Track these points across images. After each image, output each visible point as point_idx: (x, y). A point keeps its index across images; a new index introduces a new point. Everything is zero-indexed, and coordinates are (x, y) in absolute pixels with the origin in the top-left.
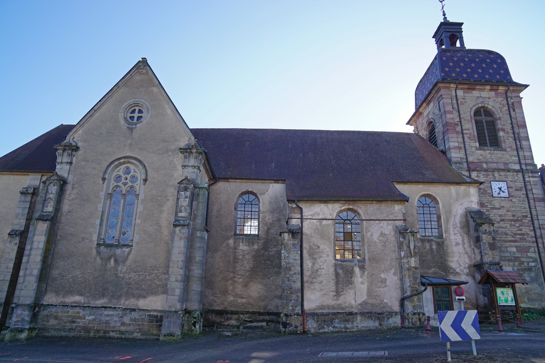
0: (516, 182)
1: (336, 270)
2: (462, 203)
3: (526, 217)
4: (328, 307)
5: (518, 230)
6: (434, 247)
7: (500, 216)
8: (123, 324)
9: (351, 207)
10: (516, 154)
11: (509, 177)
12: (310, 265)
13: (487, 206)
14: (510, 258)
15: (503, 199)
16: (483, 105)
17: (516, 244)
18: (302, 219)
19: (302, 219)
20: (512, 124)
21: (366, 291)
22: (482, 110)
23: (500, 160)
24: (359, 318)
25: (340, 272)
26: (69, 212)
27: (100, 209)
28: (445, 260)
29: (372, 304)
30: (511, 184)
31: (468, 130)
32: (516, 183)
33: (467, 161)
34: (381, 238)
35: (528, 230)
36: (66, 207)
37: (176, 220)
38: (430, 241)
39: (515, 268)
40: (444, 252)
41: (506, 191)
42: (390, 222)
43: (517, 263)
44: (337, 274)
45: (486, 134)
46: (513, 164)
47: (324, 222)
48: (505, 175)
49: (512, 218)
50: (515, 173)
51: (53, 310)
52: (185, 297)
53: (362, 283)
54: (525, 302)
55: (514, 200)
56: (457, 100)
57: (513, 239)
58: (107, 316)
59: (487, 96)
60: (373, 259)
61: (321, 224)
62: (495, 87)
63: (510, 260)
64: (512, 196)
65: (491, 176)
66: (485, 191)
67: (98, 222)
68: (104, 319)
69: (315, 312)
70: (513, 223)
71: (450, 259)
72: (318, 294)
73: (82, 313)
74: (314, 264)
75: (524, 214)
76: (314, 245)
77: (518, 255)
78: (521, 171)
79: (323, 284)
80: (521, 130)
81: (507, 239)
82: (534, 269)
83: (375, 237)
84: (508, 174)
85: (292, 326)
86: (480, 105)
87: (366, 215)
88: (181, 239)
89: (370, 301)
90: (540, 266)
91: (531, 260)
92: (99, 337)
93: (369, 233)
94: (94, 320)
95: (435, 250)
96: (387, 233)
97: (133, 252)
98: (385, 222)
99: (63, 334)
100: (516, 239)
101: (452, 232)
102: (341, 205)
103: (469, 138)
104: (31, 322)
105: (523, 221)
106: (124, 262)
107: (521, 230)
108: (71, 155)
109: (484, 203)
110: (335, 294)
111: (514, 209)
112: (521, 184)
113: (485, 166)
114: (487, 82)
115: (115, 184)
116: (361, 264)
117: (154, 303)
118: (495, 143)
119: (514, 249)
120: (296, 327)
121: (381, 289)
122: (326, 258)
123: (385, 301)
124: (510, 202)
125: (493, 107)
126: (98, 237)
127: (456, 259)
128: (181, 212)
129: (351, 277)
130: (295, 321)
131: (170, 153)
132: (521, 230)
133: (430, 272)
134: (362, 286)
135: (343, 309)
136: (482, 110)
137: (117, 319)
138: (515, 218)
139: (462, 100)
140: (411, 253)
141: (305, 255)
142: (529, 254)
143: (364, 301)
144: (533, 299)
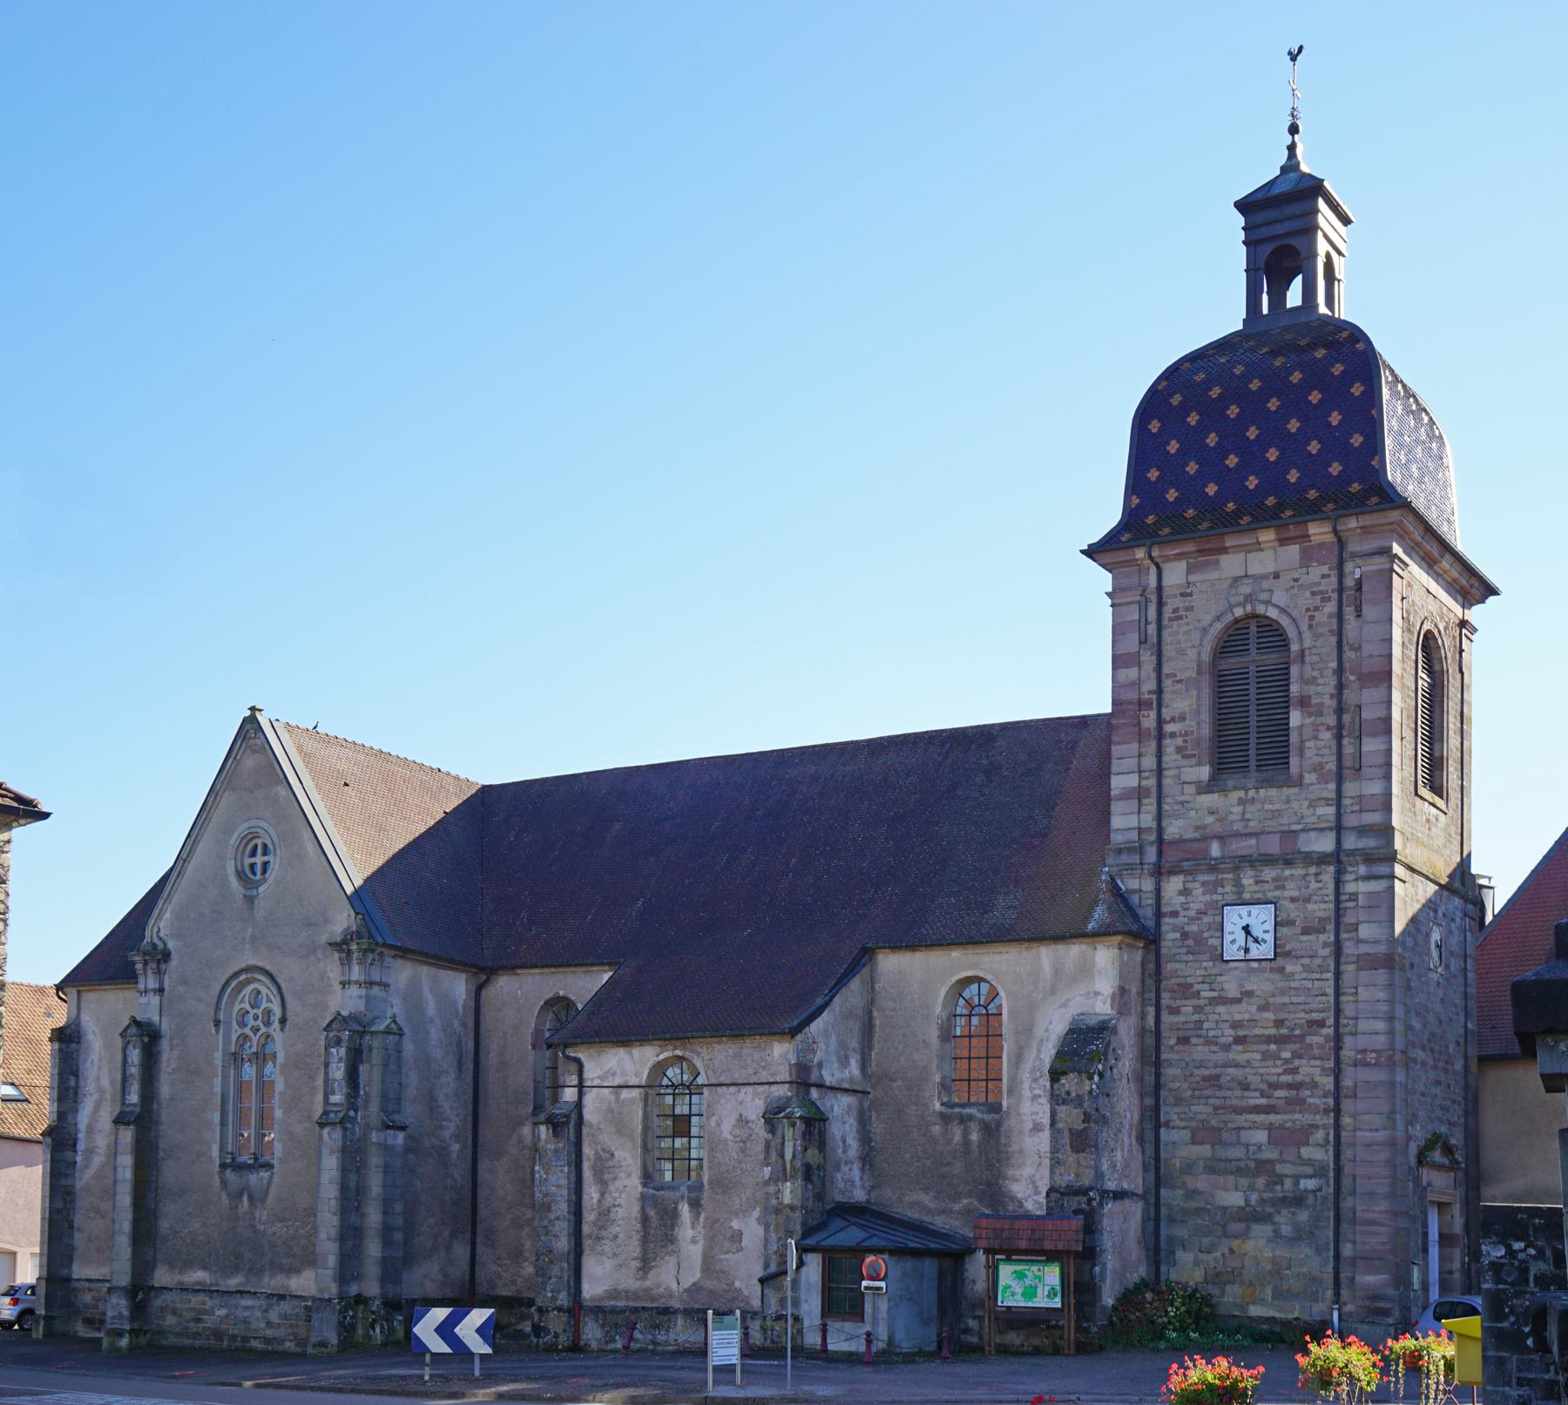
0: (1308, 900)
1: (643, 1208)
2: (1068, 1001)
3: (1321, 1024)
4: (628, 1294)
5: (1286, 1072)
6: (974, 1137)
7: (1236, 1025)
8: (269, 1324)
9: (679, 1053)
10: (1333, 795)
11: (1290, 885)
12: (596, 1196)
13: (1197, 994)
14: (1242, 1164)
15: (1255, 965)
16: (1249, 608)
17: (1273, 1118)
18: (581, 1087)
19: (581, 1087)
20: (1340, 671)
21: (699, 1260)
22: (1253, 629)
23: (1271, 824)
24: (680, 1321)
25: (652, 1213)
26: (172, 1099)
27: (218, 1089)
28: (1001, 1175)
29: (711, 1291)
30: (1292, 911)
31: (1182, 718)
32: (1310, 907)
33: (1160, 841)
34: (737, 1131)
35: (1317, 1071)
36: (165, 1089)
37: (326, 1113)
38: (964, 1120)
39: (1254, 1197)
40: (998, 1152)
41: (1270, 937)
42: (761, 1089)
43: (1261, 1182)
44: (645, 1219)
45: (1253, 724)
46: (1313, 835)
47: (625, 1094)
48: (1275, 880)
49: (1273, 1031)
50: (1313, 870)
51: (168, 1297)
52: (348, 1268)
53: (694, 1241)
54: (1262, 1302)
55: (1289, 969)
56: (1160, 604)
57: (1263, 1101)
58: (246, 1308)
59: (1271, 568)
60: (723, 1184)
61: (617, 1099)
62: (1293, 531)
63: (1240, 1172)
64: (1287, 954)
65: (1228, 888)
66: (1200, 941)
67: (217, 1118)
68: (241, 1314)
69: (602, 1304)
70: (1273, 1047)
71: (1010, 1172)
72: (609, 1264)
73: (209, 1303)
74: (602, 1194)
75: (1315, 1016)
76: (604, 1150)
77: (1270, 1154)
78: (1337, 859)
79: (619, 1241)
80: (1370, 695)
81: (1243, 1103)
82: (1311, 1199)
83: (727, 1129)
84: (1287, 872)
85: (548, 1333)
86: (1239, 612)
87: (710, 1073)
88: (331, 1152)
89: (708, 1284)
90: (1331, 1190)
91: (1309, 1170)
92: (236, 1350)
93: (714, 1119)
94: (227, 1316)
95: (974, 1148)
96: (752, 1117)
97: (275, 1179)
98: (749, 1089)
99: (187, 1342)
100: (1272, 1102)
101: (1027, 1093)
102: (658, 1050)
103: (1179, 750)
104: (132, 1319)
105: (1308, 1039)
106: (263, 1201)
107: (1295, 1071)
108: (159, 973)
109: (1192, 985)
110: (639, 1265)
111: (1286, 1000)
112: (1321, 909)
113: (1215, 850)
114: (1264, 518)
115: (240, 1031)
116: (694, 1195)
117: (305, 1283)
118: (1274, 757)
119: (1261, 1136)
120: (556, 1336)
121: (729, 1256)
122: (627, 1182)
123: (737, 1284)
124: (1277, 977)
125: (1283, 610)
126: (221, 1150)
127: (1028, 1171)
128: (333, 1093)
129: (672, 1227)
130: (556, 1324)
131: (319, 954)
132: (1295, 1071)
133: (956, 1207)
134: (693, 1247)
135: (653, 1299)
136: (1253, 629)
137: (259, 1314)
138: (1284, 1031)
139: (1179, 602)
140: (785, 1169)
141: (587, 1173)
142: (1305, 1152)
143: (695, 1284)
144: (1289, 1291)
